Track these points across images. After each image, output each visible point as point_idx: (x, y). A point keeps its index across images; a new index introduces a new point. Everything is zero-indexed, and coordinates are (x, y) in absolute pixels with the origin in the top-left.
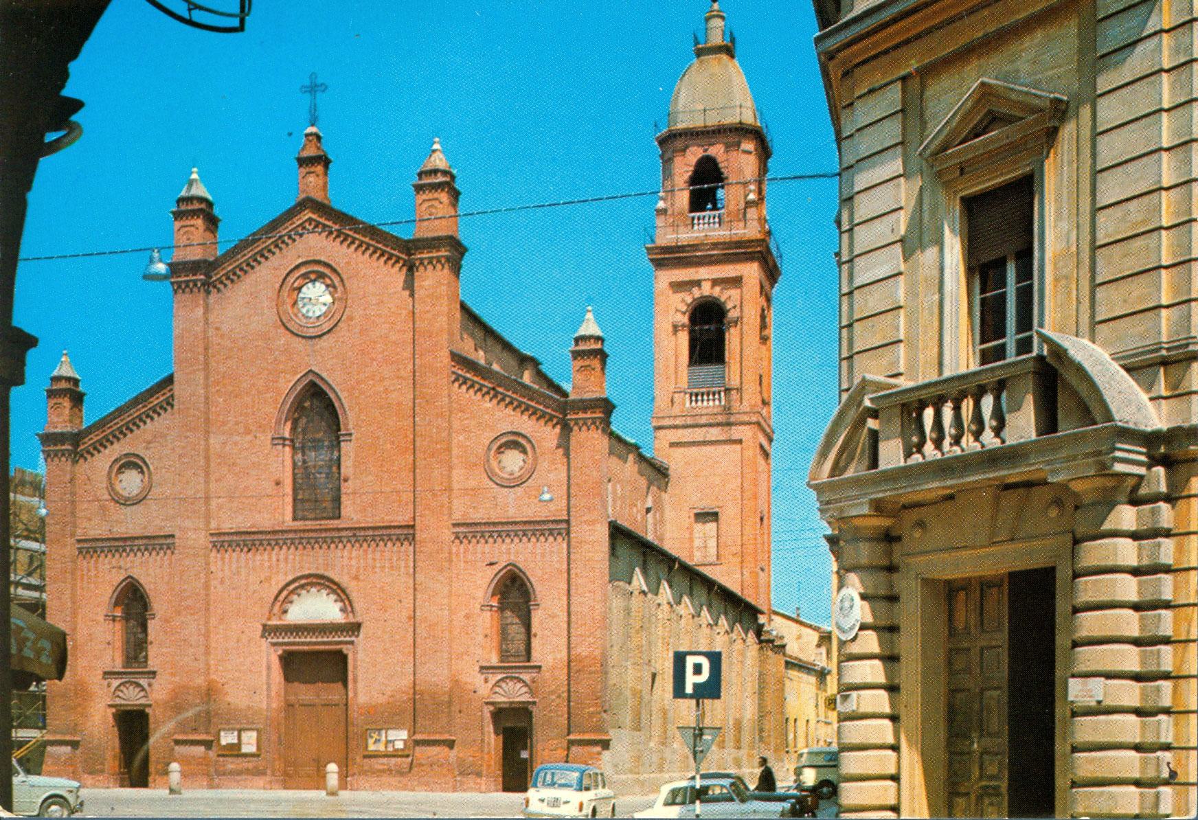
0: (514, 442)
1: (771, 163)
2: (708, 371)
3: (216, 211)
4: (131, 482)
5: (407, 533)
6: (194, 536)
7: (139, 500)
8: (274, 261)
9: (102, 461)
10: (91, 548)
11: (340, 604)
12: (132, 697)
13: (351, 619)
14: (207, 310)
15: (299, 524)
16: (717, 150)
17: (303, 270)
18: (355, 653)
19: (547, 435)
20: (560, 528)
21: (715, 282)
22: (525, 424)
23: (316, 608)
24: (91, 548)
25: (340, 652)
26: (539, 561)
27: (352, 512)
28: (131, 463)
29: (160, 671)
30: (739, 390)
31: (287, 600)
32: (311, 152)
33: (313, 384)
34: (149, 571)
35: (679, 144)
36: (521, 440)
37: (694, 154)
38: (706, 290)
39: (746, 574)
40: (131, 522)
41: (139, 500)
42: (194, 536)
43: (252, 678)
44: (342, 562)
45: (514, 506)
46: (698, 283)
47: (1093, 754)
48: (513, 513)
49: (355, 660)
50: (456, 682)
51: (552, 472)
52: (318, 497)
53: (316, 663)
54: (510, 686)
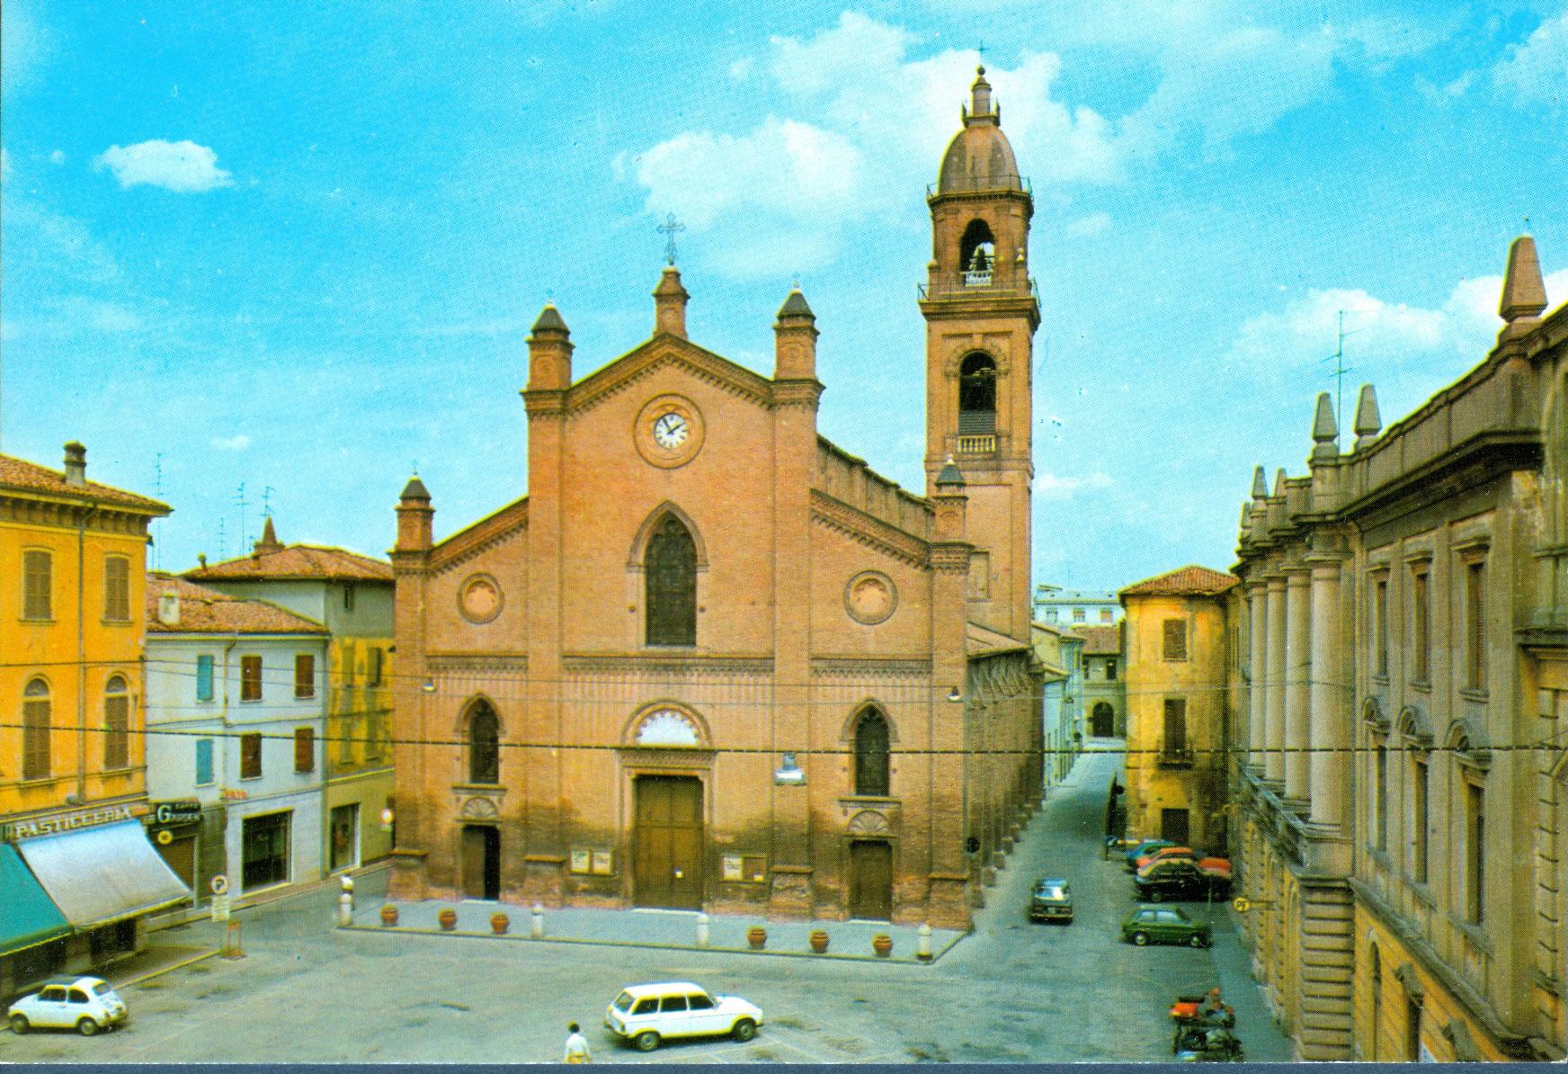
0: (874, 579)
1: (1033, 221)
2: (979, 416)
3: (572, 339)
4: (481, 600)
5: (762, 664)
6: (545, 654)
7: (488, 619)
8: (631, 392)
9: (451, 581)
10: (442, 663)
11: (694, 730)
12: (483, 811)
13: (707, 745)
14: (563, 436)
15: (653, 649)
16: (987, 213)
17: (661, 402)
18: (711, 781)
19: (909, 575)
20: (924, 665)
21: (986, 335)
22: (887, 564)
23: (668, 731)
24: (442, 663)
25: (695, 779)
26: (900, 700)
27: (706, 636)
28: (478, 581)
29: (510, 788)
30: (1009, 437)
31: (642, 724)
32: (671, 288)
33: (669, 513)
34: (502, 690)
35: (950, 206)
36: (881, 579)
37: (966, 215)
38: (977, 342)
39: (1015, 609)
40: (480, 640)
41: (488, 619)
42: (545, 654)
43: (607, 801)
44: (699, 689)
45: (873, 642)
46: (970, 335)
47: (1375, 811)
48: (871, 648)
49: (711, 787)
50: (814, 816)
51: (911, 614)
52: (671, 616)
53: (667, 782)
54: (867, 818)
